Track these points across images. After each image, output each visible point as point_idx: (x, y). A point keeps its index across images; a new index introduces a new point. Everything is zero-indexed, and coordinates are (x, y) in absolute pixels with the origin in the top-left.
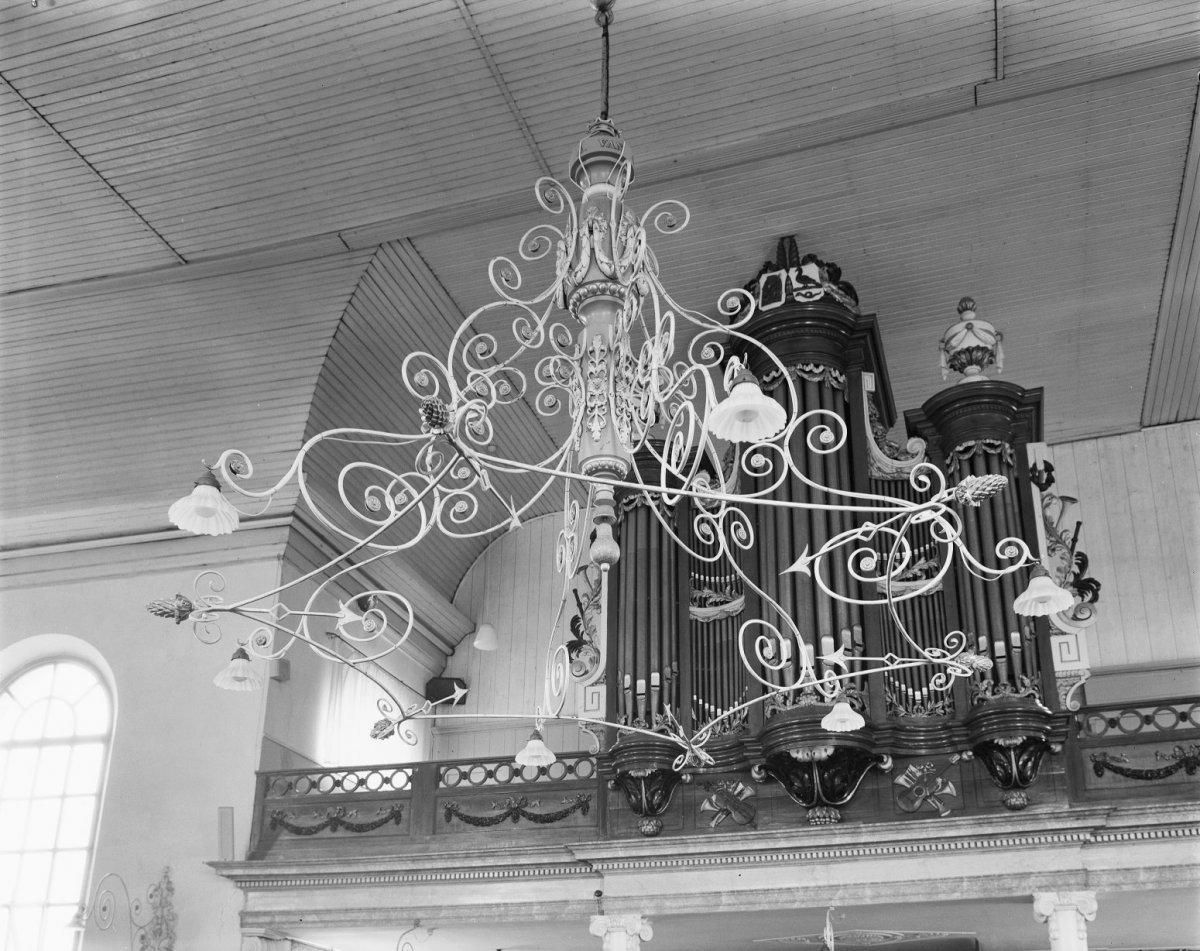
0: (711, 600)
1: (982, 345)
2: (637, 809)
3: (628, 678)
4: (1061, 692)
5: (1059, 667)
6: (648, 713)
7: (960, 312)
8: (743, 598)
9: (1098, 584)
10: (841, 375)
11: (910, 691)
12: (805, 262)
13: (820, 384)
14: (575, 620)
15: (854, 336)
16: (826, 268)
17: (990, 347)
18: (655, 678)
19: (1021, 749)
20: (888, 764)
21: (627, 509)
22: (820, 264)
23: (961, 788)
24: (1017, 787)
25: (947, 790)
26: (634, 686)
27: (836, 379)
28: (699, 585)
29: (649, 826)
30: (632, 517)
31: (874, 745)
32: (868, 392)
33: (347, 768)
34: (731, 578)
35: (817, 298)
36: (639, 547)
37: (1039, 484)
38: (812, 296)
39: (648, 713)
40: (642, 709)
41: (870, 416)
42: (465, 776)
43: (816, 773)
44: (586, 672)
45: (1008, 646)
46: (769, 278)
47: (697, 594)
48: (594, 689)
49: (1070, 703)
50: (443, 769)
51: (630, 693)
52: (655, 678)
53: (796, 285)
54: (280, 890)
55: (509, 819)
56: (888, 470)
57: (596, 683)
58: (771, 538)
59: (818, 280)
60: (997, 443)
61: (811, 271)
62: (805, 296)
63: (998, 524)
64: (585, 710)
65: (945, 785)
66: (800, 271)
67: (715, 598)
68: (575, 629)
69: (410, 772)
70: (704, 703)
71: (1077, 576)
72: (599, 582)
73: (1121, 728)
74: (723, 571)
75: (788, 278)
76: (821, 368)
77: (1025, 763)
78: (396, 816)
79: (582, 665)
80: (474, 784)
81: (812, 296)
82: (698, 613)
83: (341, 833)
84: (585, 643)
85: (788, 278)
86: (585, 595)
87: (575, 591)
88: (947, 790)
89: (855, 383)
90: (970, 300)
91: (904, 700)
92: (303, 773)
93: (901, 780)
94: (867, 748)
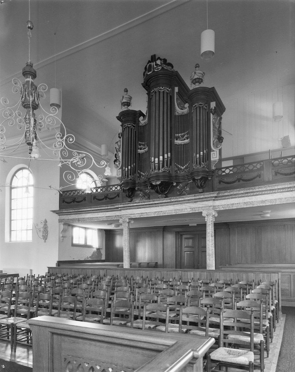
0: (143, 148)
1: (198, 77)
2: (198, 187)
4: (212, 165)
5: (212, 159)
6: (128, 175)
7: (196, 68)
8: (189, 139)
9: (223, 138)
10: (169, 88)
11: (181, 167)
12: (157, 59)
13: (163, 92)
15: (173, 78)
16: (163, 60)
17: (200, 77)
18: (129, 167)
19: (201, 179)
20: (175, 184)
22: (161, 60)
23: (190, 189)
24: (200, 188)
25: (187, 189)
26: (125, 169)
27: (168, 90)
28: (140, 145)
29: (201, 190)
30: (125, 129)
31: (171, 180)
32: (176, 92)
34: (177, 135)
35: (160, 69)
37: (212, 113)
38: (158, 69)
39: (128, 175)
40: (127, 174)
41: (177, 99)
42: (116, 188)
43: (158, 187)
44: (118, 166)
45: (200, 155)
46: (149, 65)
47: (140, 147)
48: (120, 170)
49: (213, 168)
51: (195, 158)
52: (129, 167)
53: (155, 66)
54: (244, 197)
55: (237, 181)
56: (180, 113)
57: (120, 169)
59: (160, 64)
60: (202, 103)
61: (159, 62)
62: (157, 69)
63: (201, 124)
65: (187, 188)
66: (156, 62)
68: (116, 157)
70: (140, 172)
72: (120, 145)
73: (257, 168)
75: (153, 65)
76: (164, 88)
77: (202, 183)
78: (118, 195)
79: (117, 165)
81: (158, 69)
83: (241, 182)
84: (118, 160)
85: (153, 65)
86: (118, 149)
87: (116, 148)
88: (187, 189)
89: (173, 90)
90: (198, 64)
91: (179, 169)
92: (72, 191)
93: (178, 187)
94: (169, 181)
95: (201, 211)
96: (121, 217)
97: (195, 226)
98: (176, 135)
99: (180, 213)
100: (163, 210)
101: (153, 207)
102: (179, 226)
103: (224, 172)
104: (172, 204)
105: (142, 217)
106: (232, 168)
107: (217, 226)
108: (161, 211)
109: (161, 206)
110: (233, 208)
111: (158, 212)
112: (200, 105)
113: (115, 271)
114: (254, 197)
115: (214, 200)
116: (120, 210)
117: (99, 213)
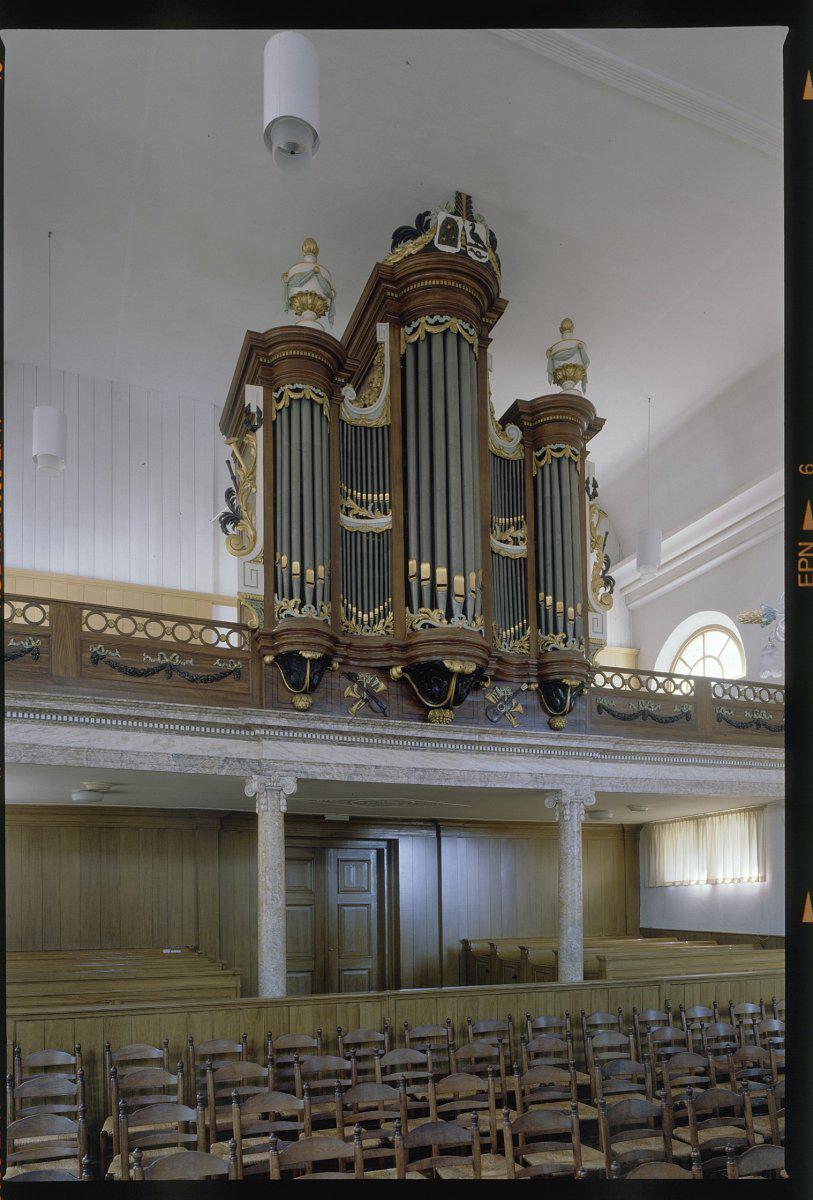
3: (285, 559)
14: (229, 493)
21: (293, 395)
29: (302, 702)
33: (92, 605)
36: (304, 441)
50: (85, 613)
53: (470, 240)
58: (293, 472)
63: (288, 510)
64: (257, 587)
67: (357, 509)
69: (46, 608)
71: (605, 572)
74: (376, 488)
80: (92, 630)
82: (350, 522)
95: (561, 787)
96: (259, 767)
97: (344, 823)
98: (387, 498)
99: (498, 786)
100: (442, 767)
101: (403, 747)
102: (166, 810)
103: (677, 687)
104: (284, 737)
105: (356, 779)
106: (665, 679)
107: (292, 820)
108: (435, 770)
109: (434, 749)
110: (634, 791)
111: (424, 770)
112: (554, 454)
113: (433, 1001)
114: (665, 767)
115: (594, 759)
116: (257, 738)
117: (131, 734)
